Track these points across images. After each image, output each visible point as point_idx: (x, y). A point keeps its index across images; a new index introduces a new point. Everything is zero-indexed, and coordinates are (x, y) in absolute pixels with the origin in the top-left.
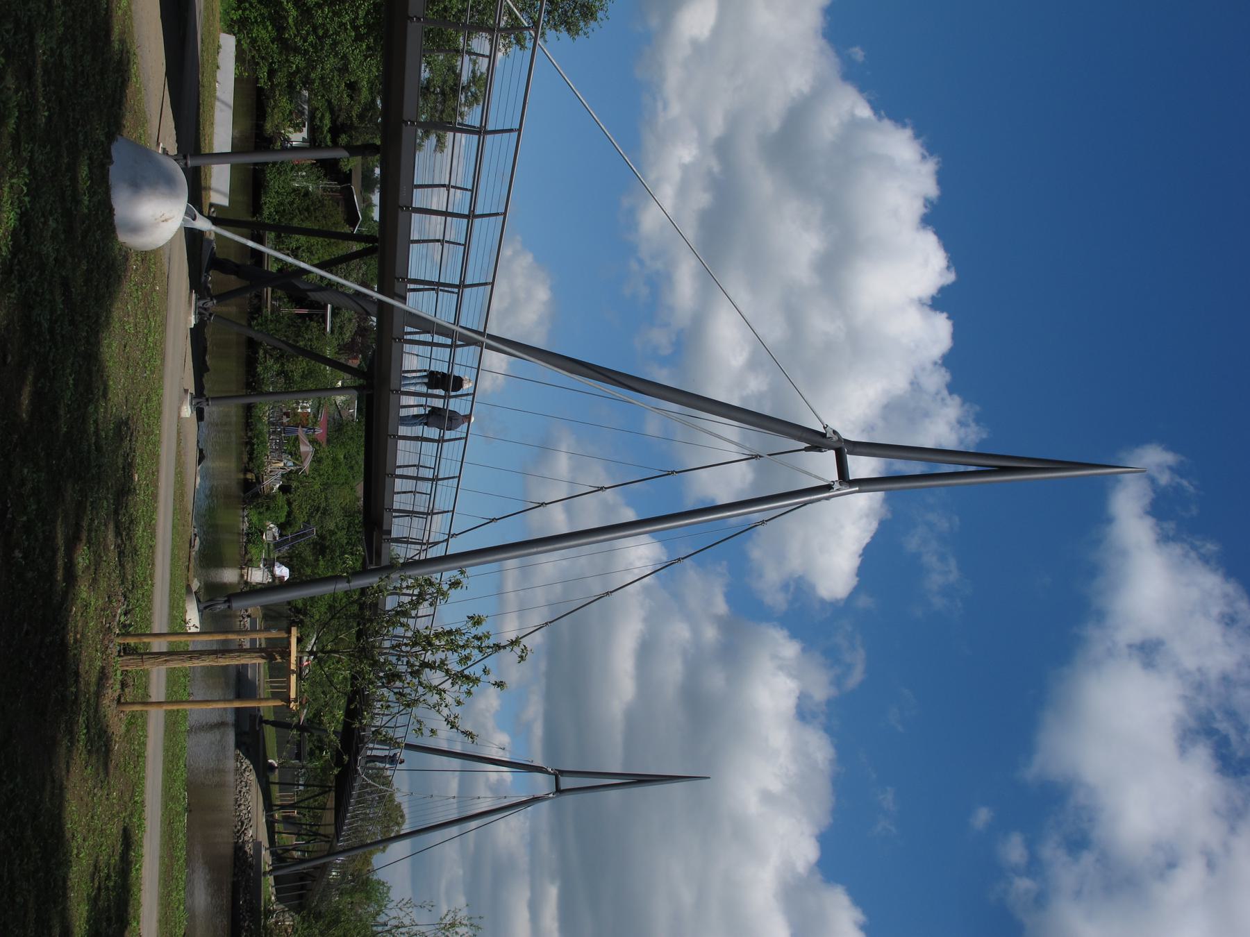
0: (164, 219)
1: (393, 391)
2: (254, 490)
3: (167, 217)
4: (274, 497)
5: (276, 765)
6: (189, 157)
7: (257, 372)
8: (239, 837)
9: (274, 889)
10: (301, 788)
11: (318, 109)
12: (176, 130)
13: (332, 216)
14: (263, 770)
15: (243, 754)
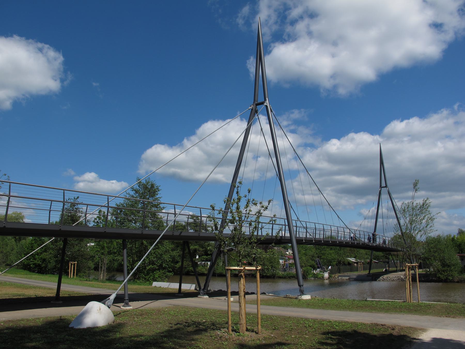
0: (99, 310)
3: (99, 309)
5: (385, 269)
6: (125, 299)
7: (269, 276)
8: (403, 280)
9: (424, 269)
10: (398, 261)
11: (201, 259)
12: (134, 301)
14: (387, 272)
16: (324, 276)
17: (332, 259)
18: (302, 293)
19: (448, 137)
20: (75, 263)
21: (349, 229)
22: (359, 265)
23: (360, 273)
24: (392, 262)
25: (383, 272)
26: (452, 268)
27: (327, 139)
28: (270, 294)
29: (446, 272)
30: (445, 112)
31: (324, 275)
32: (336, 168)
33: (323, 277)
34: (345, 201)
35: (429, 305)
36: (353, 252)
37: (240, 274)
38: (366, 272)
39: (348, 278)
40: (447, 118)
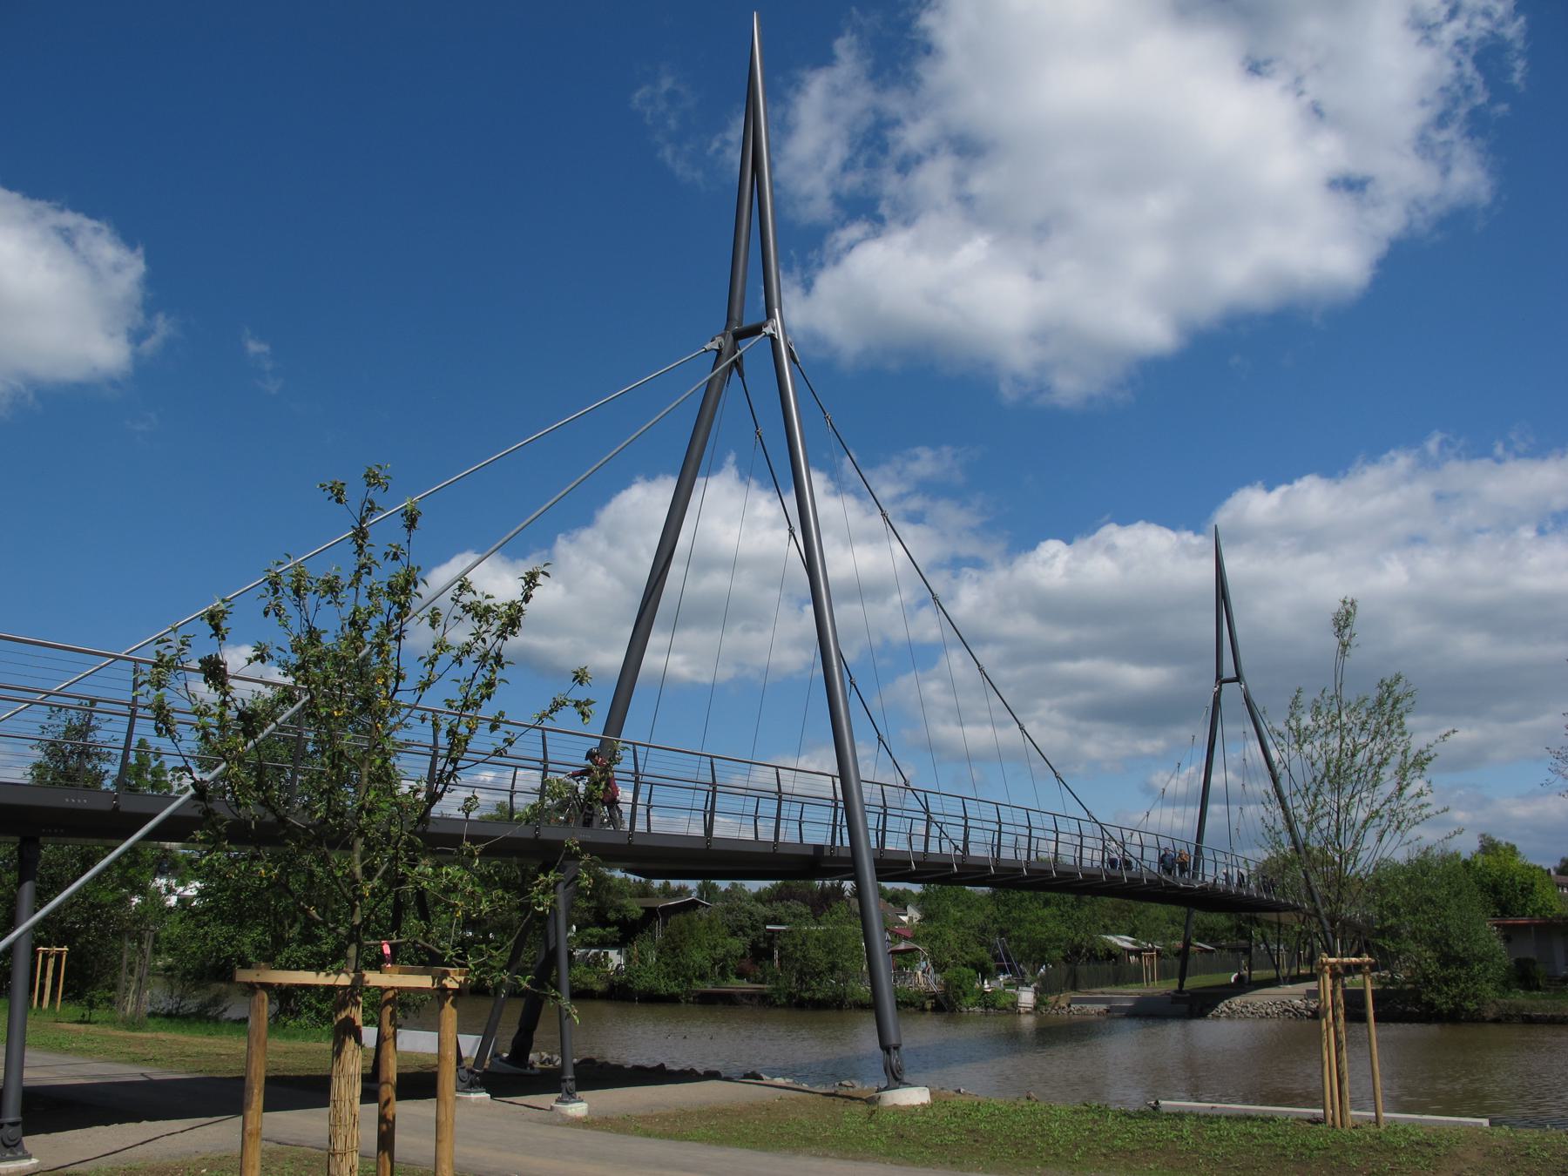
1: (708, 846)
2: (943, 1001)
4: (948, 982)
5: (1237, 974)
8: (1301, 1014)
13: (680, 925)
14: (1243, 986)
15: (1212, 1011)
16: (1017, 1002)
17: (1049, 940)
18: (896, 1078)
19: (1415, 540)
20: (63, 951)
21: (1100, 824)
22: (1146, 962)
23: (1149, 991)
24: (1262, 948)
25: (1230, 985)
26: (1473, 968)
27: (1025, 542)
28: (779, 1081)
29: (1454, 984)
30: (1402, 462)
31: (1016, 997)
32: (1062, 636)
33: (1015, 1004)
34: (1101, 744)
35: (1429, 1145)
36: (1126, 913)
37: (343, 1015)
38: (1172, 985)
39: (1103, 1007)
40: (1408, 479)
